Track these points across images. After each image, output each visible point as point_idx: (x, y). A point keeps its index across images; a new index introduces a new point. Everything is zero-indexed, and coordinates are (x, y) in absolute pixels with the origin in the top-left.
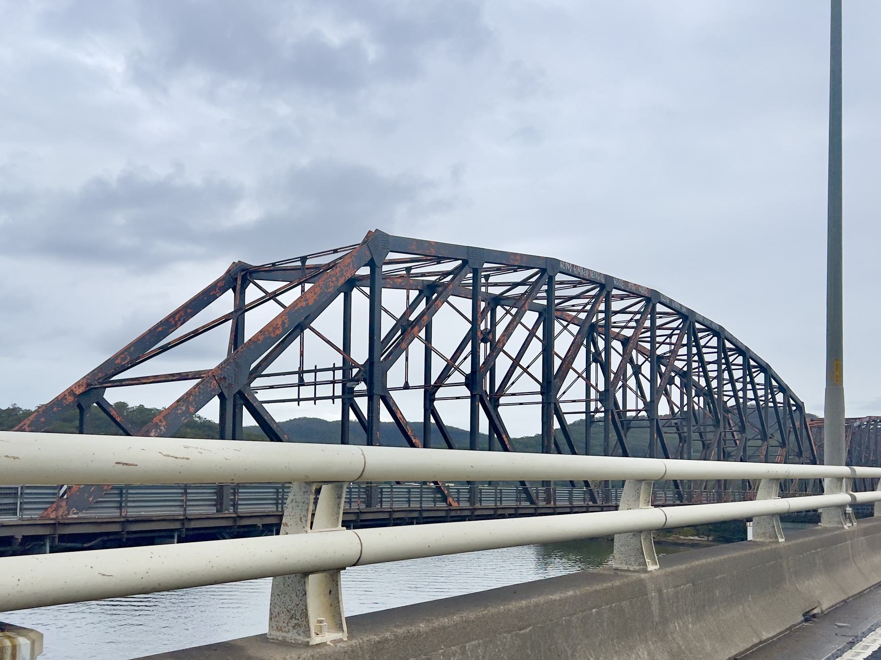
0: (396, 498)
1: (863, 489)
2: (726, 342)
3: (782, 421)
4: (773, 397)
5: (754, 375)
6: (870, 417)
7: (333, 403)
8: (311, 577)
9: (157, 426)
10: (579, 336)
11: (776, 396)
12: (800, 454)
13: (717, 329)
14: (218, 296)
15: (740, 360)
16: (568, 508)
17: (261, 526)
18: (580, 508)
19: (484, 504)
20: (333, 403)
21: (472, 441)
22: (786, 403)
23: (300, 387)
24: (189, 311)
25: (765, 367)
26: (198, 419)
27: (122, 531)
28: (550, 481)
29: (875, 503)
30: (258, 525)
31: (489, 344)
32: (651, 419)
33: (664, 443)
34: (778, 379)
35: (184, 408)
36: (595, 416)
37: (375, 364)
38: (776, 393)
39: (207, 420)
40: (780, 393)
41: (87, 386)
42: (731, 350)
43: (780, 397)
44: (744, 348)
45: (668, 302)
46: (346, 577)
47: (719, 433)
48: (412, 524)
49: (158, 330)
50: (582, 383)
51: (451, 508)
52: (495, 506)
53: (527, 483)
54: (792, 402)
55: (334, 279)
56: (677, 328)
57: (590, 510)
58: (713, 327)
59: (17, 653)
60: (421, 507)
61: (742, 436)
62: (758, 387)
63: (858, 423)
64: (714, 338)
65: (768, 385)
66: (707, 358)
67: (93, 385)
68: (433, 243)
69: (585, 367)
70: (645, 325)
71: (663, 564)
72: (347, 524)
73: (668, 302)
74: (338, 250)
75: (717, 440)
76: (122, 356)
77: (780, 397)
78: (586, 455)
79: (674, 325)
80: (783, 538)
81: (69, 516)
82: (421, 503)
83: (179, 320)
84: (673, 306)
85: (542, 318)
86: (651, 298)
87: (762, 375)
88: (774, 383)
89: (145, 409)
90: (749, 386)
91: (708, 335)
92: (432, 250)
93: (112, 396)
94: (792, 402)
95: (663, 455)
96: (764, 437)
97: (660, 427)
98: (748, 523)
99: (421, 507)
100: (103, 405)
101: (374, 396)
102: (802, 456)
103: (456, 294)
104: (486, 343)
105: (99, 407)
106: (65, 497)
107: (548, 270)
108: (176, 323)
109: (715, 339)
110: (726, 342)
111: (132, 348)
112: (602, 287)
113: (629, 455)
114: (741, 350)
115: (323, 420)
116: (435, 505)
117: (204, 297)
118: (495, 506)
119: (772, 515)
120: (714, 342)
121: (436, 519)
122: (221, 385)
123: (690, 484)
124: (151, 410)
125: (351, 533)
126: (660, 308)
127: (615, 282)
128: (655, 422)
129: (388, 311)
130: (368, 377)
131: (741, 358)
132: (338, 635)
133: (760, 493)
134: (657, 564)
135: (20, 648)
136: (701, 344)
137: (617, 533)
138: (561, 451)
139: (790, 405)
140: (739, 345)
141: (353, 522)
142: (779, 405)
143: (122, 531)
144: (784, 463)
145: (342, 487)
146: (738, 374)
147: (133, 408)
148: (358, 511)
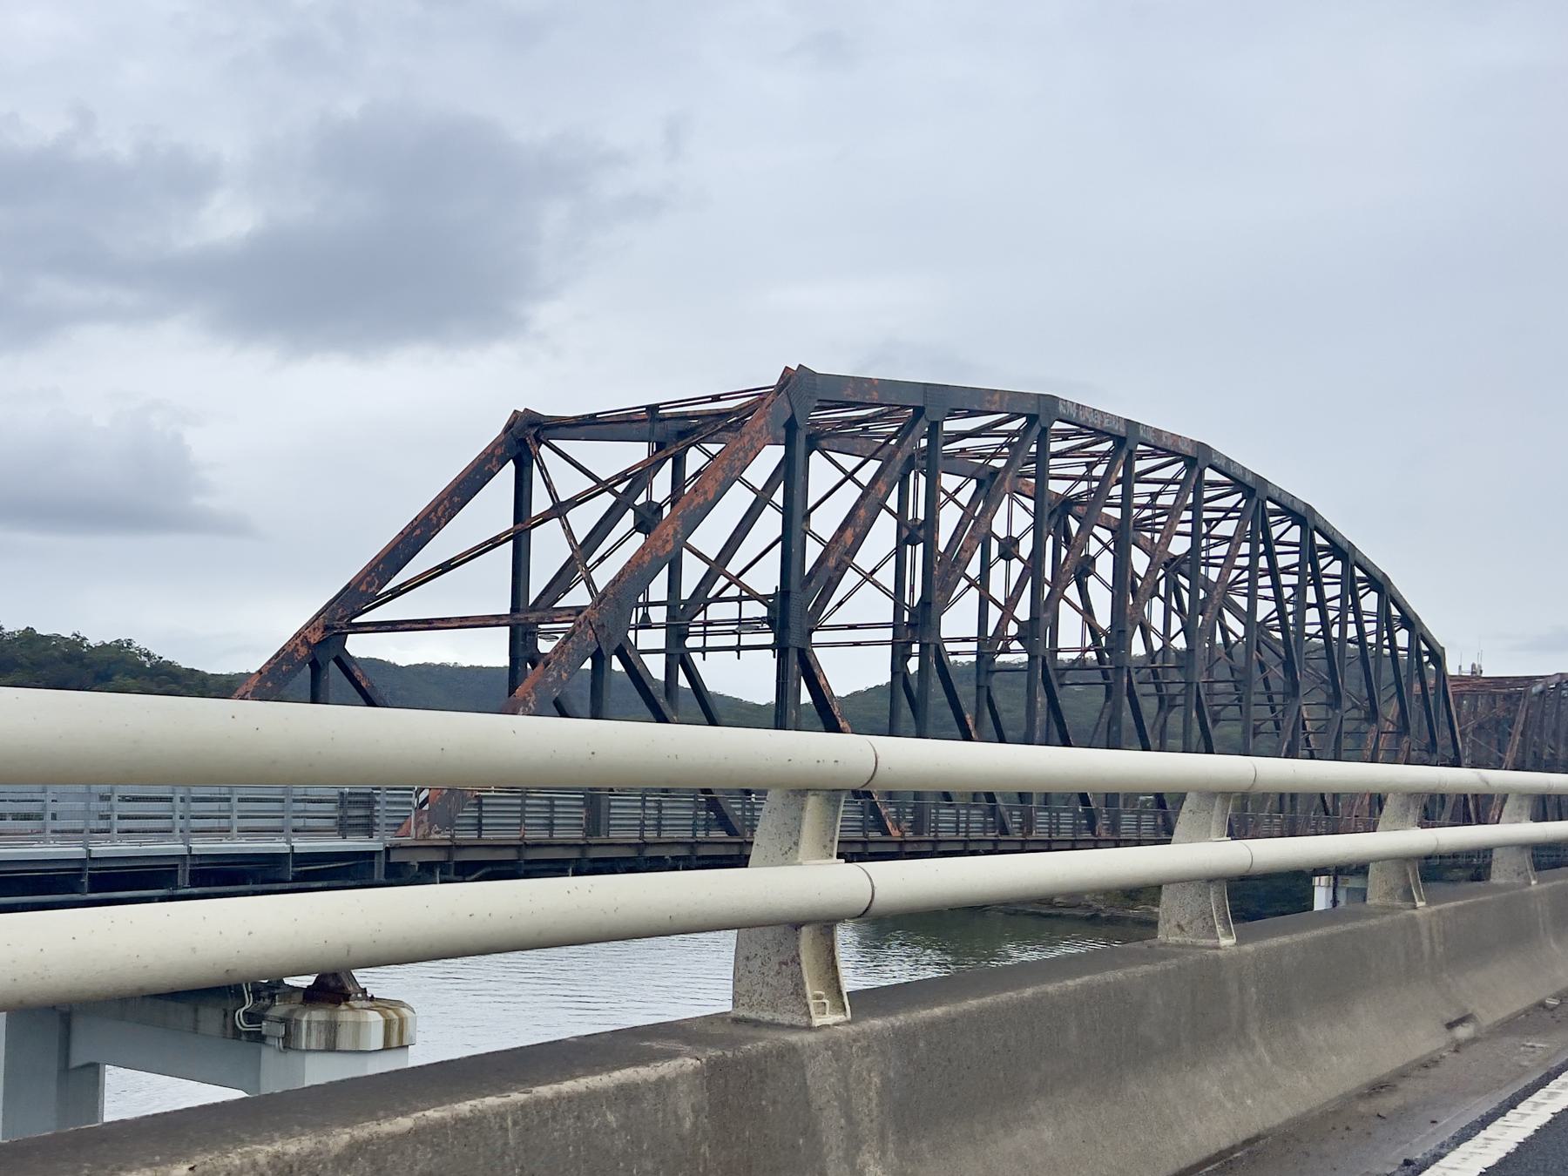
0: (615, 819)
1: (1556, 816)
2: (1317, 535)
3: (1404, 681)
4: (1392, 638)
5: (1361, 593)
6: (1561, 674)
7: (704, 659)
8: (804, 929)
9: (525, 702)
10: (1082, 533)
11: (1397, 634)
12: (1432, 747)
13: (1302, 510)
14: (495, 471)
15: (1336, 568)
16: (927, 844)
17: (417, 865)
18: (849, 845)
19: (616, 835)
20: (704, 659)
21: (781, 716)
22: (1413, 649)
23: (639, 631)
24: (456, 499)
25: (1380, 580)
26: (146, 659)
27: (519, 860)
28: (1032, 794)
29: (1371, 864)
30: (412, 864)
31: (920, 547)
32: (1117, 667)
33: (989, 708)
34: (1402, 604)
35: (555, 673)
36: (997, 660)
37: (791, 595)
38: (1396, 629)
39: (164, 661)
40: (1403, 630)
41: (325, 630)
42: (1322, 548)
43: (1402, 638)
44: (1345, 546)
45: (1223, 464)
46: (78, 1025)
47: (1297, 708)
48: (676, 869)
49: (414, 534)
50: (974, 593)
51: (590, 842)
52: (901, 837)
53: (998, 798)
54: (1424, 648)
55: (741, 454)
56: (1234, 509)
57: (1078, 846)
58: (1296, 507)
59: (405, 1032)
60: (641, 837)
61: (1335, 713)
62: (1365, 618)
63: (1539, 687)
64: (1294, 527)
65: (1383, 617)
66: (1282, 561)
67: (336, 628)
68: (876, 382)
69: (895, 546)
70: (1031, 451)
71: (1429, 904)
72: (849, 857)
73: (1223, 464)
74: (721, 397)
75: (1294, 719)
76: (368, 579)
77: (1402, 638)
78: (920, 736)
79: (1229, 502)
80: (1423, 901)
81: (432, 837)
82: (642, 831)
83: (443, 516)
84: (1232, 471)
85: (984, 491)
86: (1196, 458)
87: (1374, 596)
88: (1395, 612)
89: (38, 635)
90: (1351, 617)
91: (1282, 521)
92: (875, 393)
93: (358, 646)
94: (1424, 648)
95: (958, 733)
96: (1373, 715)
97: (1134, 682)
98: (1317, 878)
99: (641, 837)
100: (345, 664)
101: (790, 649)
102: (1436, 752)
103: (846, 450)
104: (914, 544)
105: (695, 692)
106: (426, 807)
107: (1041, 418)
108: (439, 519)
109: (1297, 529)
110: (1317, 535)
111: (381, 566)
112: (1120, 441)
113: (1152, 747)
114: (1341, 550)
115: (388, 663)
116: (479, 836)
117: (475, 476)
118: (965, 836)
119: (1211, 880)
120: (1294, 534)
121: (718, 862)
122: (598, 636)
123: (1245, 801)
124: (48, 638)
125: (855, 868)
126: (1210, 475)
127: (1141, 432)
128: (1195, 688)
129: (751, 489)
130: (778, 617)
131: (1339, 564)
132: (840, 1018)
133: (763, 840)
134: (1231, 934)
135: (407, 1022)
136: (1051, 450)
137: (1372, 862)
138: (714, 719)
139: (1419, 653)
140: (1338, 540)
141: (852, 853)
142: (1400, 652)
143: (519, 860)
144: (1405, 764)
145: (840, 796)
146: (1331, 591)
147: (14, 633)
148: (641, 841)
